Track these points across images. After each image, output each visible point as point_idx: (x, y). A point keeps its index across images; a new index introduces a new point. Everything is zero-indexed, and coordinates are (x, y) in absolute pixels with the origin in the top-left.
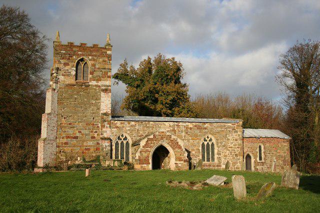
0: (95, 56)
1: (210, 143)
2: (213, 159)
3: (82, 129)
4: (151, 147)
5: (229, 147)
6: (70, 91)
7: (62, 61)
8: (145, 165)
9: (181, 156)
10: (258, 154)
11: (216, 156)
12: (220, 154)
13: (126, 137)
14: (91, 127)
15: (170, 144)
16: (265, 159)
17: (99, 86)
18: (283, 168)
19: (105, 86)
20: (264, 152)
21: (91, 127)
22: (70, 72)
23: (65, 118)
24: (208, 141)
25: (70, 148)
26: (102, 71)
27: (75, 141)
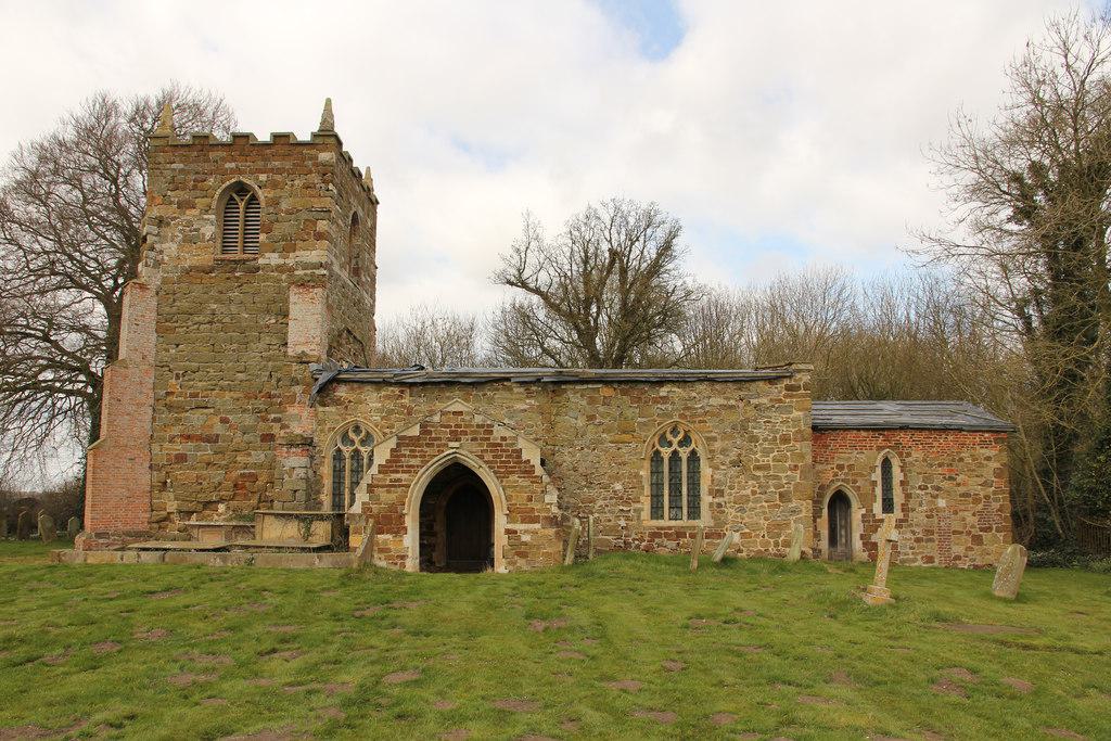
0: (279, 171)
1: (684, 453)
2: (694, 512)
3: (230, 412)
4: (410, 469)
5: (758, 468)
6: (197, 290)
7: (175, 196)
8: (389, 537)
9: (530, 505)
10: (879, 491)
11: (706, 499)
12: (720, 493)
13: (368, 434)
14: (260, 404)
15: (489, 456)
16: (905, 508)
17: (291, 270)
18: (978, 540)
19: (306, 266)
20: (902, 483)
21: (260, 404)
22: (197, 230)
23: (178, 377)
24: (675, 446)
25: (194, 474)
26: (563, 300)
27: (207, 451)
